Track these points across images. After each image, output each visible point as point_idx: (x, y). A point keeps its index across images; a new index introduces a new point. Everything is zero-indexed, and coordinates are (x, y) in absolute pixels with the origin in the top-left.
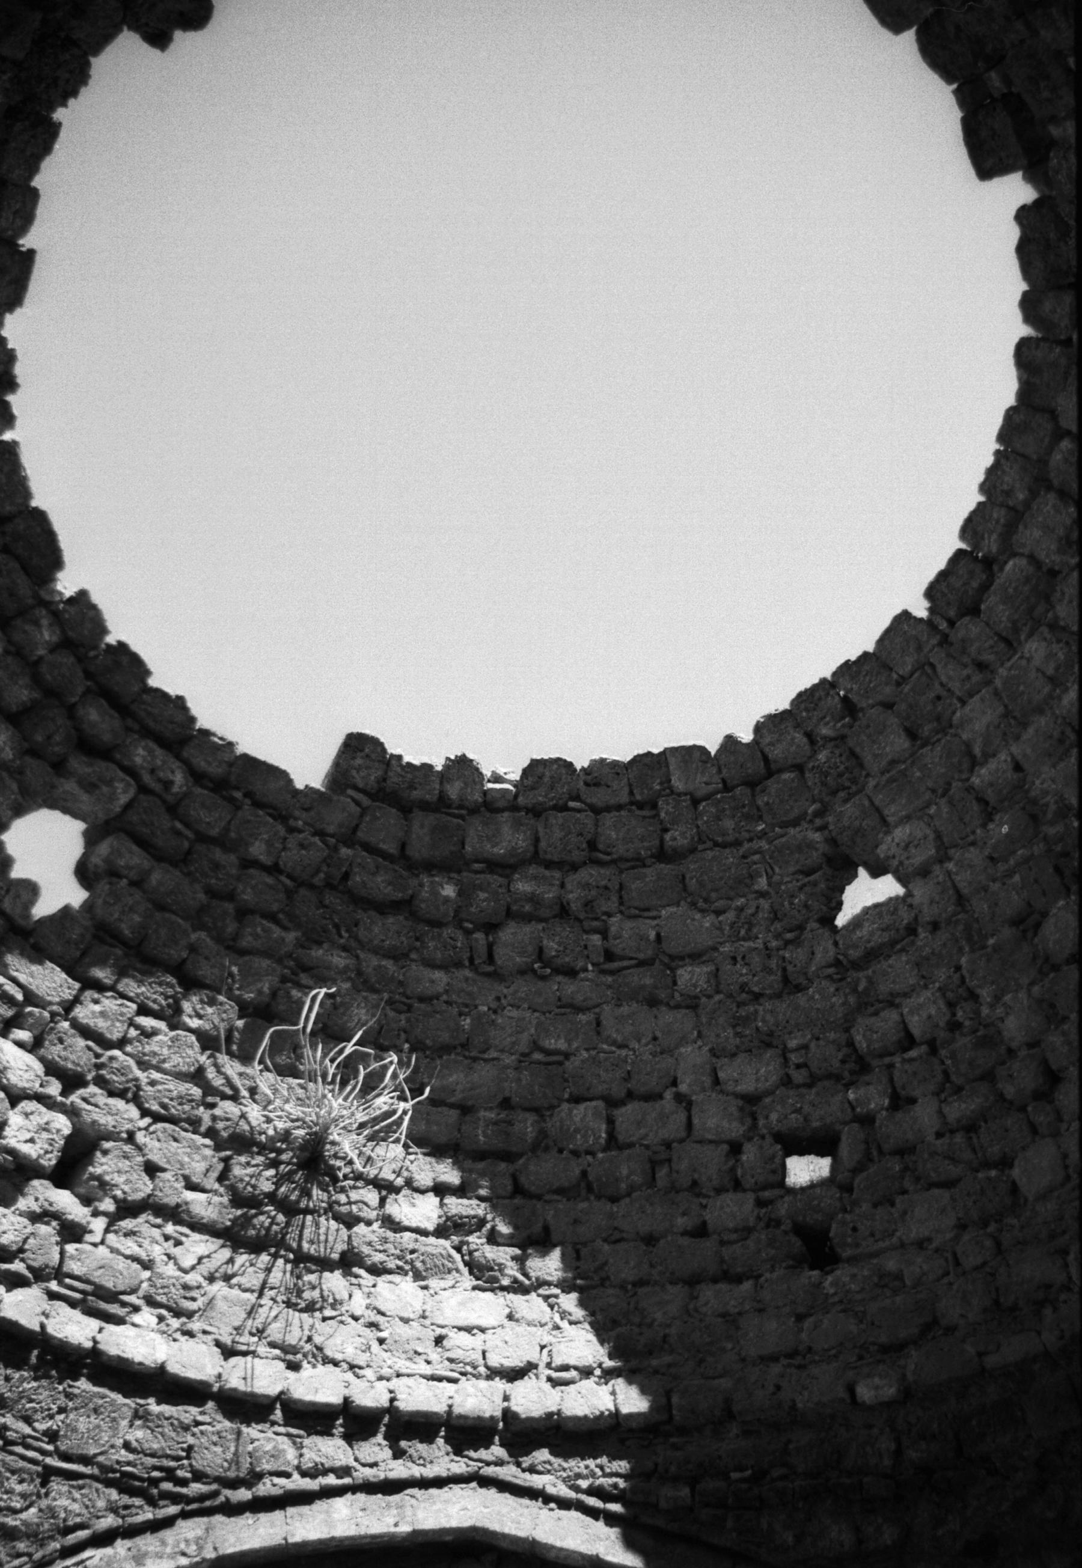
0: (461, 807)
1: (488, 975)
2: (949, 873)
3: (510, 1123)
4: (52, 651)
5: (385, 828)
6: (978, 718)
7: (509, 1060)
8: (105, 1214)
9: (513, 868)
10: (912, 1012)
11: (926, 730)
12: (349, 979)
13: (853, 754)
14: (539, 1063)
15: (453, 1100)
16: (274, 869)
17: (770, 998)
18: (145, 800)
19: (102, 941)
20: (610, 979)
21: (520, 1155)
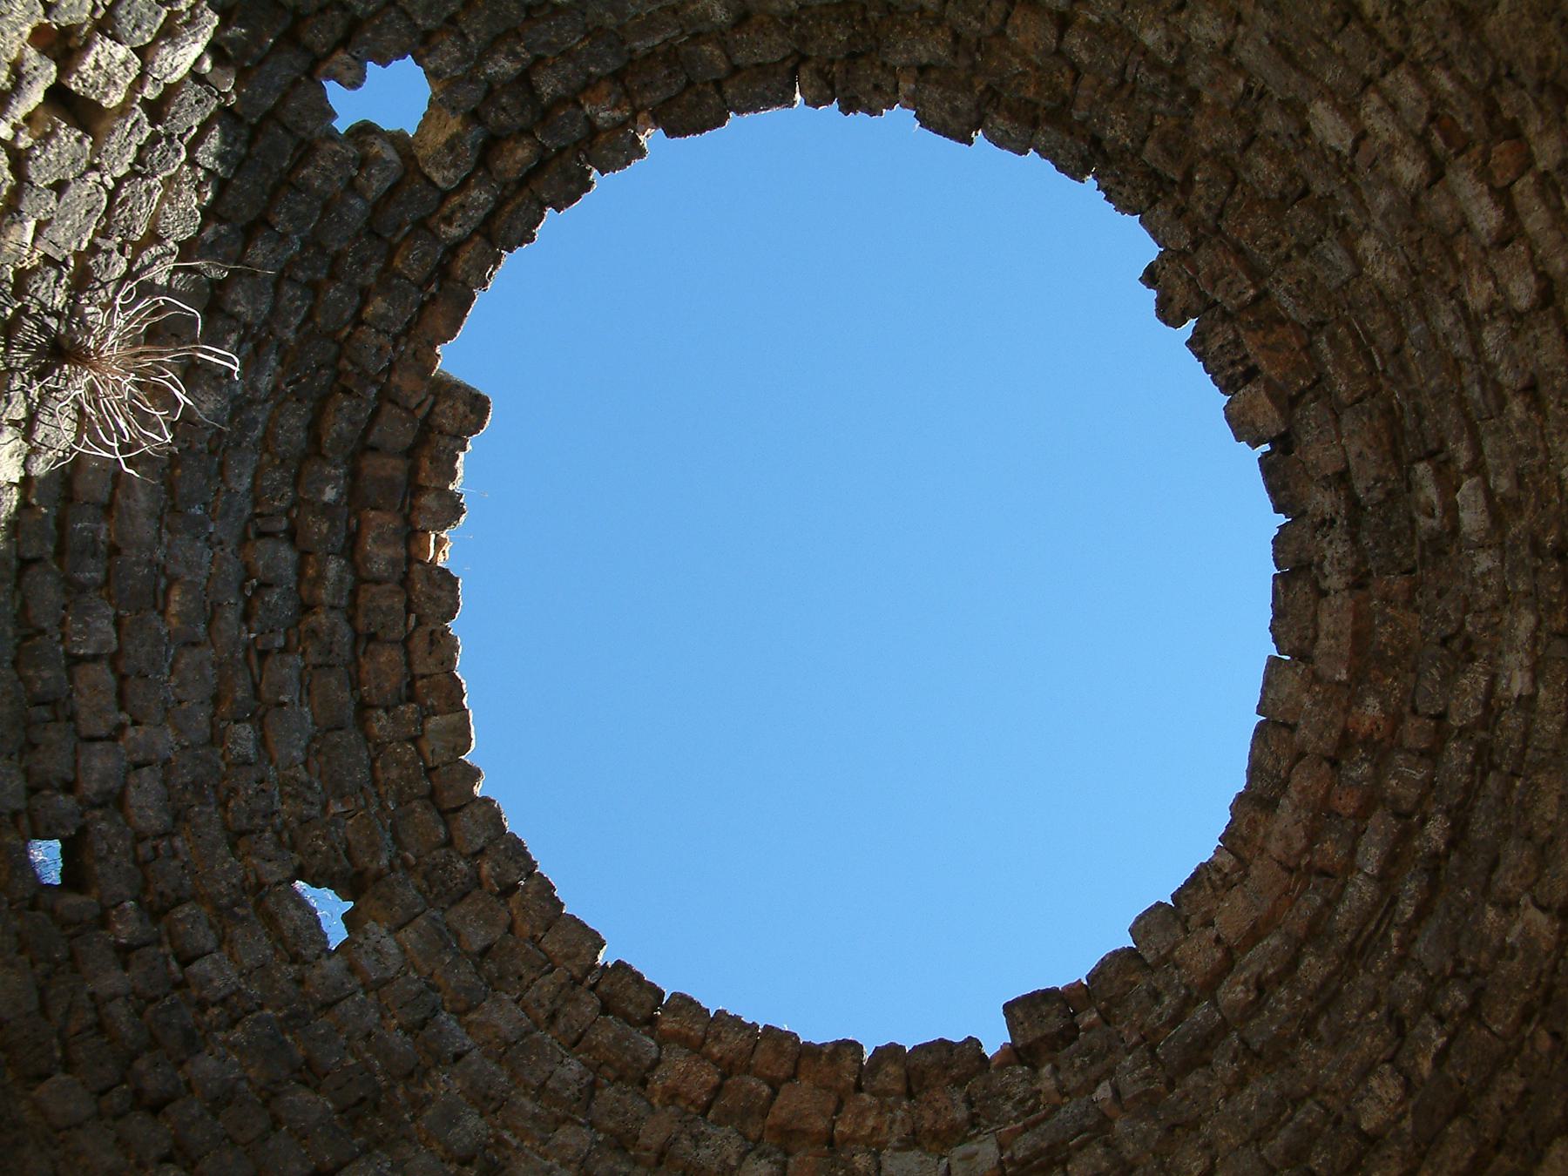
0: (412, 507)
1: (245, 531)
2: (354, 993)
3: (94, 555)
4: (587, 117)
5: (395, 431)
6: (503, 1016)
7: (159, 554)
8: (16, 137)
9: (351, 560)
10: (215, 962)
11: (490, 966)
12: (245, 393)
13: (465, 895)
14: (157, 585)
15: (119, 495)
16: (358, 321)
17: (224, 819)
18: (432, 196)
19: (297, 148)
20: (240, 655)
21: (60, 566)
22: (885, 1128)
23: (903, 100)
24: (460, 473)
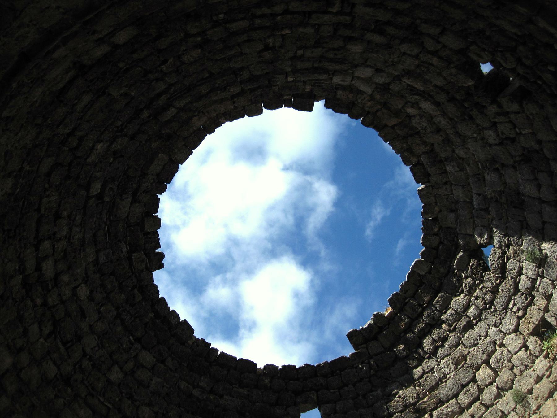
6: (458, 193)
22: (366, 99)
23: (194, 339)
24: (368, 323)
